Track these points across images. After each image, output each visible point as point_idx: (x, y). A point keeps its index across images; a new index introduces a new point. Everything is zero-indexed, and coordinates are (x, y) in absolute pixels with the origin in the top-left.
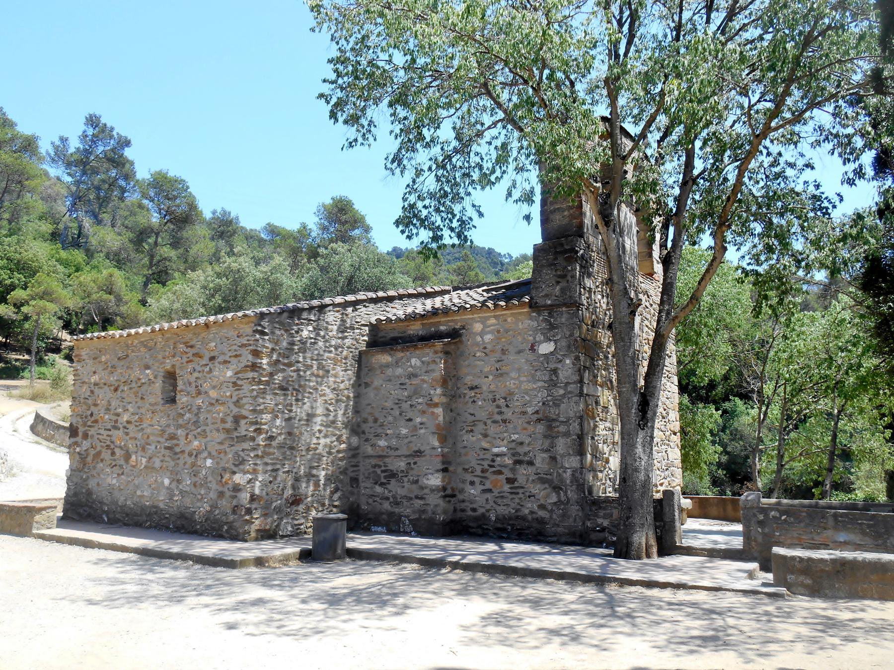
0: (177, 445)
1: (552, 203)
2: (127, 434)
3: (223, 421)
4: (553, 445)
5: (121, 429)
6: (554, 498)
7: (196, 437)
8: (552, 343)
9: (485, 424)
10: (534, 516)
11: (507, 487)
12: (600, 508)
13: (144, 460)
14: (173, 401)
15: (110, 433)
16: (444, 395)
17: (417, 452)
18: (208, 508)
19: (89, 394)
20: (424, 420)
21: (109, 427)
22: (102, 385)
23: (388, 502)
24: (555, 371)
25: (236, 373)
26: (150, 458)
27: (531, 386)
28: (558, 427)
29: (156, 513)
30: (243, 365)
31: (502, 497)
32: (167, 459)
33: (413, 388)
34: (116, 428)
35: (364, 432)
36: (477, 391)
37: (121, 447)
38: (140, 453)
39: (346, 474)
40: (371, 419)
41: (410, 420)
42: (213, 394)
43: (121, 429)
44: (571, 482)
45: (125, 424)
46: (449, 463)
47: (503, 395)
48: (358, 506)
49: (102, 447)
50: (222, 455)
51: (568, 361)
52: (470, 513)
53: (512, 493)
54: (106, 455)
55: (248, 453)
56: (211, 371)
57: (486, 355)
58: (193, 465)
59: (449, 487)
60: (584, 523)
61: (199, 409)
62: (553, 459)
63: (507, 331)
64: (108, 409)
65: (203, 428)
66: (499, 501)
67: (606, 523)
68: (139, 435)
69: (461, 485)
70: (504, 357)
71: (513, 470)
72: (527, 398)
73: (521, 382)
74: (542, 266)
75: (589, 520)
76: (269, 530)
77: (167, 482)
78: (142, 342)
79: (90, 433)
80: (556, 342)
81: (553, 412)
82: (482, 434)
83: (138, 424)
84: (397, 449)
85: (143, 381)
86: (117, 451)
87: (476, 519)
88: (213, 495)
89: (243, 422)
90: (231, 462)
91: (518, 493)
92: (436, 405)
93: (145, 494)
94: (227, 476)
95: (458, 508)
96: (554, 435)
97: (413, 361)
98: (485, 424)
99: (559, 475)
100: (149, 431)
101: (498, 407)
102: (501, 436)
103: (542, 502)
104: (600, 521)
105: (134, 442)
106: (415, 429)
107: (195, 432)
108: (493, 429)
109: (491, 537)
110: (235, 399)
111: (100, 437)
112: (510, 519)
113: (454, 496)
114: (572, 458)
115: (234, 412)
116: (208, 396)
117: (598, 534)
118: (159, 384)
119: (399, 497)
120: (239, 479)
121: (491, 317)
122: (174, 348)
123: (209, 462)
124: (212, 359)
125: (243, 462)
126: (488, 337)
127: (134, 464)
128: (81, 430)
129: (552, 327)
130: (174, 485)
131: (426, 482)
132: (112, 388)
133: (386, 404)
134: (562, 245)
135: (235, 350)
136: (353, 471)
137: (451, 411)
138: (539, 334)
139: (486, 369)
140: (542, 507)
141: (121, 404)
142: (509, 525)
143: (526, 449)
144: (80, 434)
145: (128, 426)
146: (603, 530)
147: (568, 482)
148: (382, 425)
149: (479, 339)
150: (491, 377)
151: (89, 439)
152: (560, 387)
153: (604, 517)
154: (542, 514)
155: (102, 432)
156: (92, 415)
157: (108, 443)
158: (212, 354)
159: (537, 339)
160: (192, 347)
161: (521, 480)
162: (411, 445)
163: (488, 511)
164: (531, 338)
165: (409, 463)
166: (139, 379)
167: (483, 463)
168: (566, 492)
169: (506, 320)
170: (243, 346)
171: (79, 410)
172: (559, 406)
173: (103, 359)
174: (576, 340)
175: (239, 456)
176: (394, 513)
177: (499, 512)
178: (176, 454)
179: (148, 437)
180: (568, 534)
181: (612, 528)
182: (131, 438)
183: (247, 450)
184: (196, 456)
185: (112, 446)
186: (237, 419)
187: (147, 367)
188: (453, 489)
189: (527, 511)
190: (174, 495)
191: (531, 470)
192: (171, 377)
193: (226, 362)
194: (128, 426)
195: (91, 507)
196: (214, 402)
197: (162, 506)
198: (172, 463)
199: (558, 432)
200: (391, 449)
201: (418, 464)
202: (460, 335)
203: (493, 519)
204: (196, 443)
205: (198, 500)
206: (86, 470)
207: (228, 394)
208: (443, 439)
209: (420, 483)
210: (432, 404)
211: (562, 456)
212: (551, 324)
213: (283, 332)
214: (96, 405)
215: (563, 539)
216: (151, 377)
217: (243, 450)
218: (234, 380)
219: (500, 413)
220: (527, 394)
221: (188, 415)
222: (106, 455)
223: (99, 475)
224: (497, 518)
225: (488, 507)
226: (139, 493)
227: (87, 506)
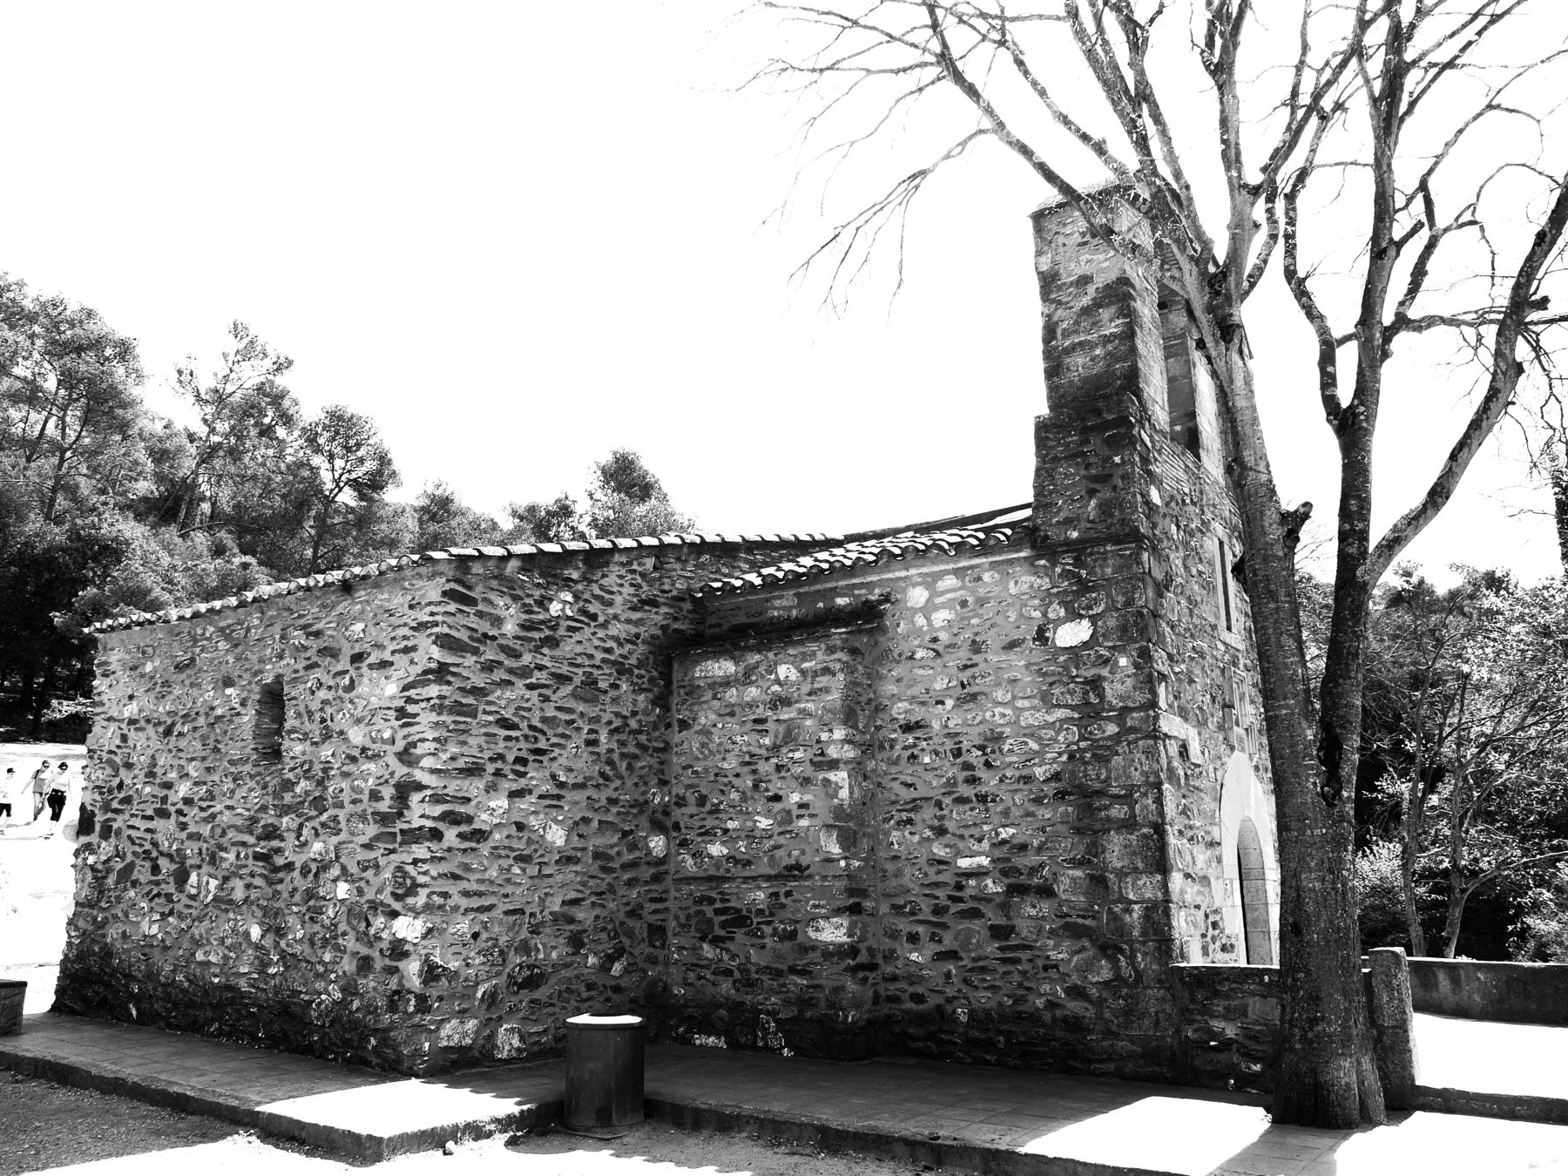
0: (279, 851)
1: (1067, 334)
2: (183, 826)
3: (375, 796)
4: (1095, 849)
5: (173, 817)
6: (1104, 972)
7: (317, 835)
8: (1086, 623)
9: (939, 805)
10: (1059, 1013)
11: (992, 948)
12: (1216, 994)
13: (213, 883)
14: (275, 754)
15: (150, 825)
16: (849, 742)
17: (789, 868)
18: (338, 995)
19: (118, 742)
20: (807, 798)
21: (150, 812)
22: (143, 723)
23: (731, 980)
24: (1095, 684)
25: (405, 688)
26: (226, 879)
28: (1107, 808)
29: (232, 1002)
30: (419, 669)
31: (983, 970)
32: (258, 881)
33: (782, 729)
34: (163, 814)
35: (677, 827)
36: (919, 734)
37: (170, 856)
38: (206, 868)
39: (640, 917)
40: (691, 798)
41: (777, 798)
42: (357, 736)
43: (173, 817)
44: (1144, 934)
45: (180, 806)
46: (863, 893)
47: (977, 743)
48: (666, 988)
49: (134, 853)
50: (369, 874)
51: (1123, 661)
52: (910, 1005)
53: (1004, 961)
54: (142, 873)
55: (425, 867)
56: (351, 687)
57: (938, 654)
58: (310, 894)
59: (862, 947)
60: (1178, 1031)
61: (325, 770)
62: (1098, 882)
63: (982, 602)
64: (151, 774)
65: (331, 812)
66: (975, 978)
67: (1231, 1032)
68: (206, 830)
69: (887, 943)
70: (977, 658)
71: (1005, 907)
72: (1034, 746)
73: (1019, 711)
74: (1056, 459)
75: (1191, 1022)
76: (469, 1048)
77: (256, 932)
78: (222, 630)
79: (115, 826)
80: (1094, 620)
81: (1093, 775)
82: (932, 828)
83: (204, 804)
84: (749, 863)
85: (219, 712)
86: (164, 863)
87: (922, 1019)
88: (348, 965)
89: (415, 798)
90: (389, 889)
91: (1017, 961)
92: (833, 765)
93: (213, 959)
94: (379, 921)
95: (883, 993)
96: (1098, 826)
97: (783, 671)
98: (939, 805)
99: (1114, 917)
100: (226, 818)
101: (968, 766)
102: (976, 832)
103: (1075, 979)
104: (1217, 1025)
105: (195, 846)
106: (787, 818)
107: (315, 823)
108: (956, 817)
110: (400, 745)
111: (134, 833)
112: (1003, 1018)
113: (873, 967)
114: (1144, 879)
115: (397, 776)
116: (346, 740)
117: (1212, 1055)
118: (248, 717)
119: (753, 969)
120: (407, 928)
121: (947, 572)
122: (282, 638)
123: (342, 890)
124: (357, 658)
125: (412, 890)
126: (941, 617)
127: (193, 891)
128: (99, 818)
129: (1084, 587)
131: (812, 934)
132: (161, 729)
133: (726, 766)
134: (1098, 413)
135: (405, 638)
136: (655, 912)
137: (865, 777)
138: (1055, 606)
139: (939, 685)
140: (1076, 992)
141: (176, 762)
142: (1000, 1032)
143: (1032, 859)
144: (98, 827)
145: (186, 809)
146: (1226, 1045)
147: (1135, 933)
148: (716, 810)
149: (920, 621)
150: (950, 703)
151: (113, 840)
152: (1108, 719)
153: (1227, 1016)
154: (1075, 1007)
155: (137, 822)
156: (120, 786)
157: (148, 846)
159: (1051, 615)
161: (1025, 929)
162: (779, 853)
163: (949, 1000)
164: (1038, 614)
165: (776, 895)
166: (212, 709)
167: (938, 893)
168: (1132, 959)
169: (979, 579)
170: (421, 626)
171: (100, 775)
172: (1107, 760)
173: (149, 668)
174: (1140, 614)
175: (405, 875)
176: (742, 1003)
177: (975, 1005)
178: (277, 870)
179: (224, 833)
180: (1142, 1056)
181: (1247, 1042)
182: (191, 837)
183: (424, 861)
184: (316, 875)
185: (154, 854)
187: (228, 682)
188: (870, 950)
189: (1040, 1003)
190: (270, 963)
191: (1045, 907)
192: (274, 699)
193: (384, 664)
194: (186, 809)
195: (108, 985)
196: (356, 753)
197: (243, 985)
198: (269, 891)
199: (1109, 819)
200: (737, 862)
201: (796, 896)
202: (881, 615)
203: (963, 1018)
204: (317, 846)
205: (318, 976)
206: (103, 904)
207: (387, 735)
208: (848, 841)
209: (800, 938)
211: (1121, 874)
212: (1080, 580)
213: (508, 600)
214: (129, 766)
215: (1129, 1067)
216: (235, 703)
217: (415, 862)
218: (401, 703)
219: (972, 781)
220: (1032, 736)
221: (303, 783)
222: (142, 873)
223: (126, 915)
224: (972, 1013)
225: (950, 992)
226: (200, 956)
227: (100, 981)
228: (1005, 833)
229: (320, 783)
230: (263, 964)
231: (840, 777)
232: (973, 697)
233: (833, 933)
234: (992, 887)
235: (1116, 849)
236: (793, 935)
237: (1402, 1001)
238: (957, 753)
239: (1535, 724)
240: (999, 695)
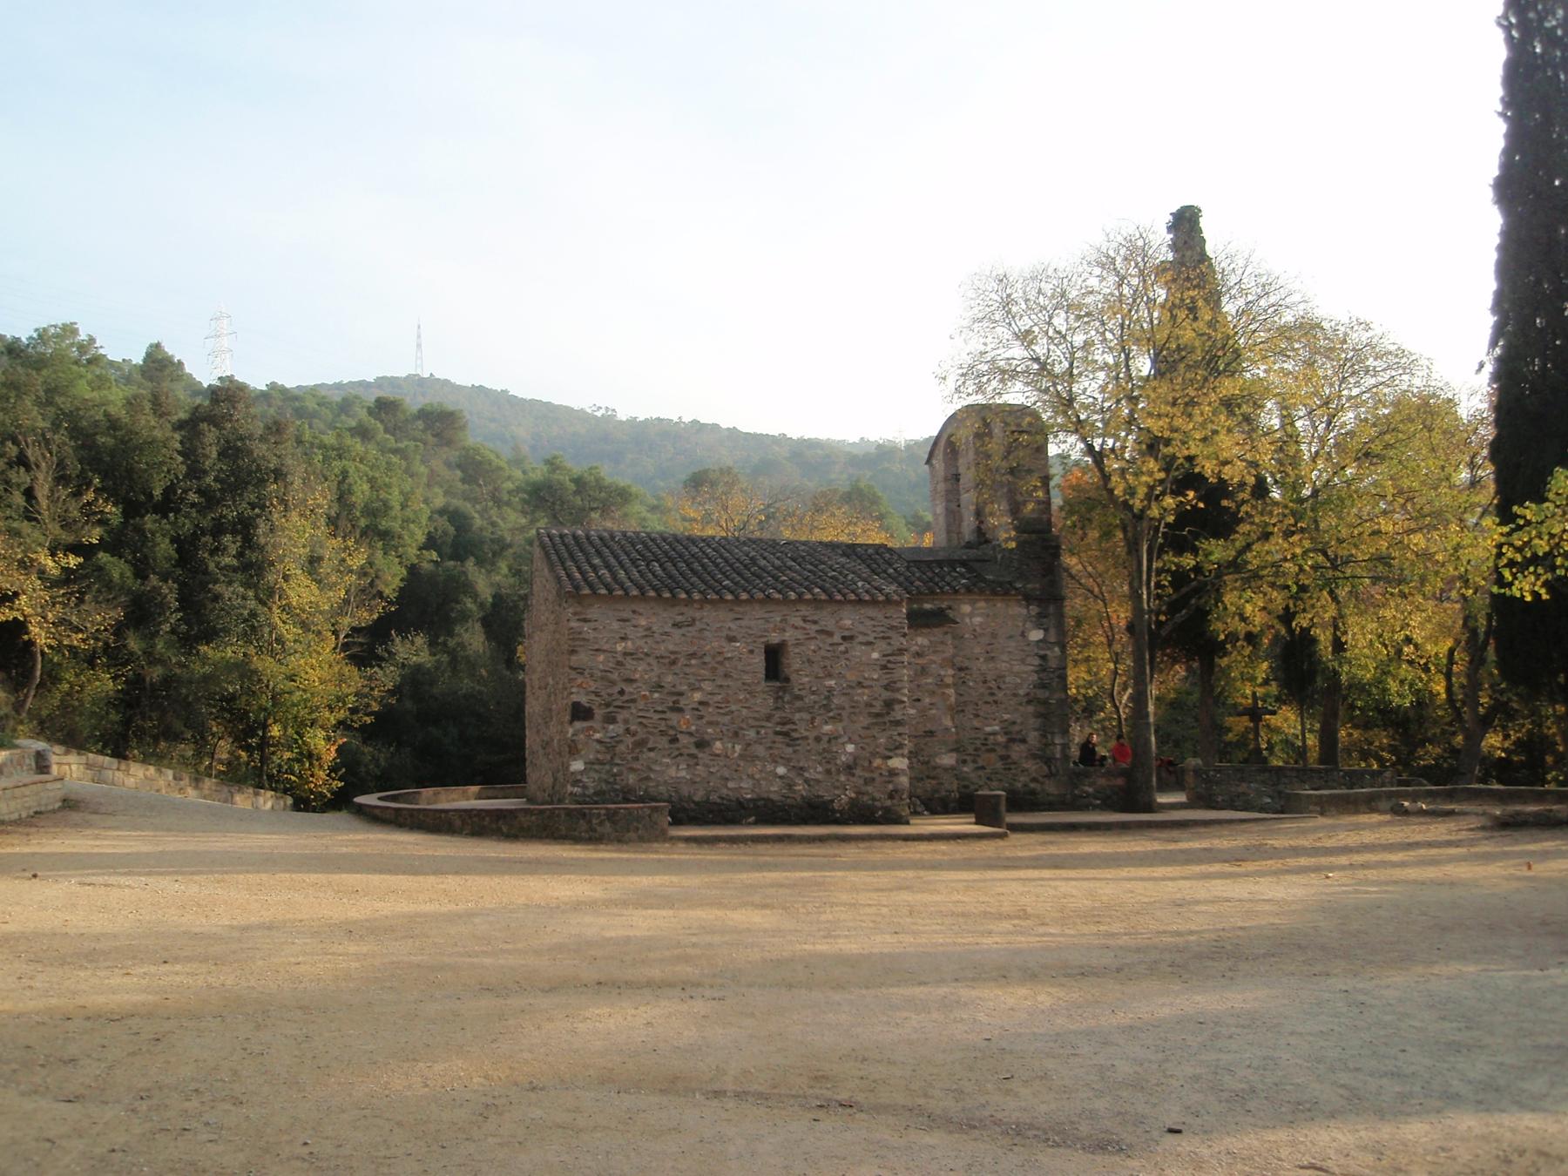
11: (999, 765)
13: (738, 748)
54: (663, 742)
67: (1091, 790)
89: (897, 707)
92: (948, 686)
123: (850, 748)
126: (977, 620)
143: (1017, 728)
146: (1088, 795)
154: (1032, 785)
156: (622, 692)
158: (846, 633)
160: (815, 622)
161: (1014, 756)
185: (672, 732)
187: (731, 639)
191: (1023, 747)
193: (869, 643)
210: (941, 683)
228: (1006, 717)
229: (827, 698)
230: (790, 786)
233: (948, 760)
234: (1001, 739)
236: (928, 763)
237: (420, 857)
238: (985, 682)
239: (881, 591)
240: (1005, 657)
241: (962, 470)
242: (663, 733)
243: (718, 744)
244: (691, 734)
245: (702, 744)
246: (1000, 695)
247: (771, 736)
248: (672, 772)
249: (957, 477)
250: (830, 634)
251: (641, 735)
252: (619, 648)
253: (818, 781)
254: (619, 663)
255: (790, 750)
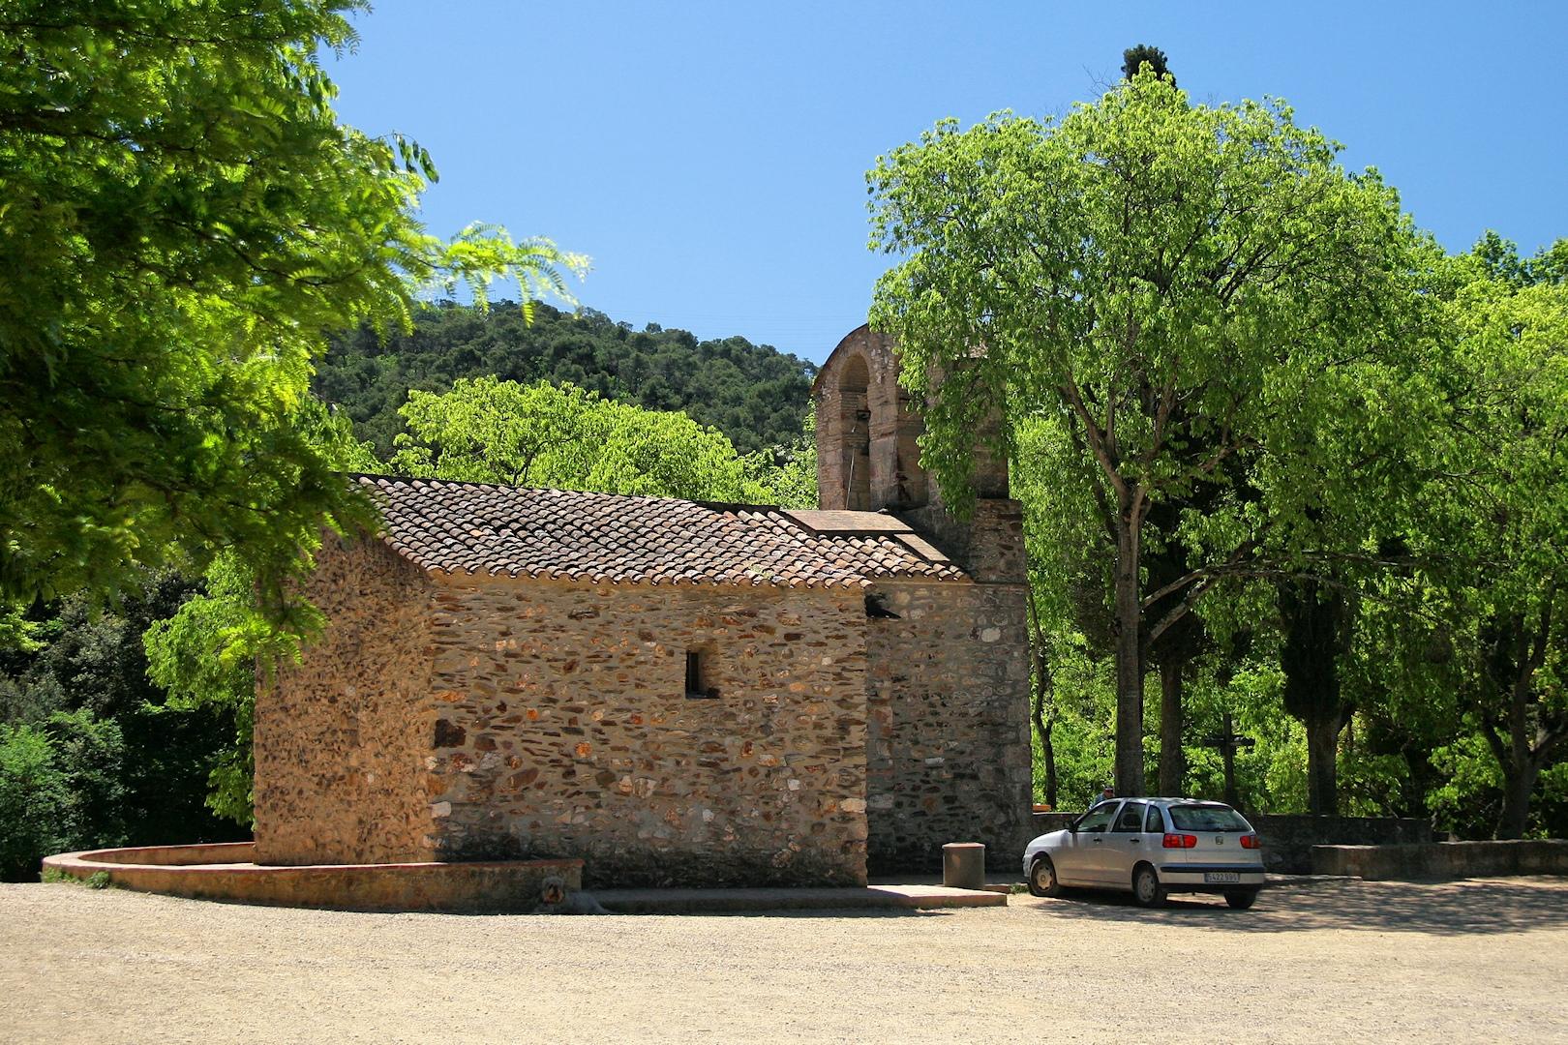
3: (818, 726)
4: (999, 755)
6: (1002, 818)
11: (943, 808)
13: (651, 784)
24: (1002, 665)
27: (973, 681)
42: (796, 687)
54: (554, 777)
62: (1000, 771)
80: (1002, 629)
81: (998, 715)
89: (853, 728)
92: (883, 702)
101: (932, 705)
103: (987, 823)
108: (924, 734)
109: (925, 873)
123: (794, 785)
130: (722, 820)
132: (560, 664)
139: (916, 656)
155: (539, 737)
156: (502, 707)
157: (555, 755)
158: (792, 630)
173: (530, 612)
184: (768, 775)
186: (843, 726)
187: (647, 637)
197: (699, 851)
211: (1011, 769)
228: (954, 744)
231: (888, 710)
232: (936, 665)
234: (947, 775)
235: (1010, 755)
241: (874, 406)
242: (555, 763)
243: (627, 779)
244: (591, 764)
245: (607, 778)
246: (944, 715)
247: (694, 768)
248: (567, 817)
249: (863, 416)
250: (770, 631)
251: (527, 765)
252: (500, 645)
253: (753, 829)
254: (501, 668)
255: (718, 788)
